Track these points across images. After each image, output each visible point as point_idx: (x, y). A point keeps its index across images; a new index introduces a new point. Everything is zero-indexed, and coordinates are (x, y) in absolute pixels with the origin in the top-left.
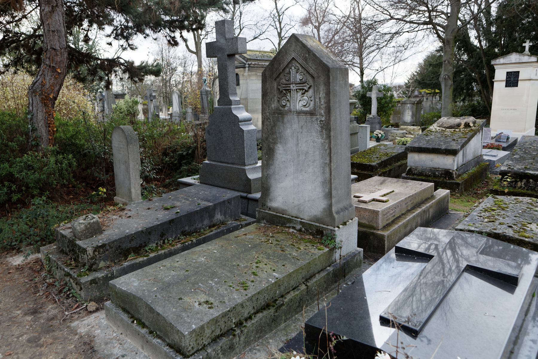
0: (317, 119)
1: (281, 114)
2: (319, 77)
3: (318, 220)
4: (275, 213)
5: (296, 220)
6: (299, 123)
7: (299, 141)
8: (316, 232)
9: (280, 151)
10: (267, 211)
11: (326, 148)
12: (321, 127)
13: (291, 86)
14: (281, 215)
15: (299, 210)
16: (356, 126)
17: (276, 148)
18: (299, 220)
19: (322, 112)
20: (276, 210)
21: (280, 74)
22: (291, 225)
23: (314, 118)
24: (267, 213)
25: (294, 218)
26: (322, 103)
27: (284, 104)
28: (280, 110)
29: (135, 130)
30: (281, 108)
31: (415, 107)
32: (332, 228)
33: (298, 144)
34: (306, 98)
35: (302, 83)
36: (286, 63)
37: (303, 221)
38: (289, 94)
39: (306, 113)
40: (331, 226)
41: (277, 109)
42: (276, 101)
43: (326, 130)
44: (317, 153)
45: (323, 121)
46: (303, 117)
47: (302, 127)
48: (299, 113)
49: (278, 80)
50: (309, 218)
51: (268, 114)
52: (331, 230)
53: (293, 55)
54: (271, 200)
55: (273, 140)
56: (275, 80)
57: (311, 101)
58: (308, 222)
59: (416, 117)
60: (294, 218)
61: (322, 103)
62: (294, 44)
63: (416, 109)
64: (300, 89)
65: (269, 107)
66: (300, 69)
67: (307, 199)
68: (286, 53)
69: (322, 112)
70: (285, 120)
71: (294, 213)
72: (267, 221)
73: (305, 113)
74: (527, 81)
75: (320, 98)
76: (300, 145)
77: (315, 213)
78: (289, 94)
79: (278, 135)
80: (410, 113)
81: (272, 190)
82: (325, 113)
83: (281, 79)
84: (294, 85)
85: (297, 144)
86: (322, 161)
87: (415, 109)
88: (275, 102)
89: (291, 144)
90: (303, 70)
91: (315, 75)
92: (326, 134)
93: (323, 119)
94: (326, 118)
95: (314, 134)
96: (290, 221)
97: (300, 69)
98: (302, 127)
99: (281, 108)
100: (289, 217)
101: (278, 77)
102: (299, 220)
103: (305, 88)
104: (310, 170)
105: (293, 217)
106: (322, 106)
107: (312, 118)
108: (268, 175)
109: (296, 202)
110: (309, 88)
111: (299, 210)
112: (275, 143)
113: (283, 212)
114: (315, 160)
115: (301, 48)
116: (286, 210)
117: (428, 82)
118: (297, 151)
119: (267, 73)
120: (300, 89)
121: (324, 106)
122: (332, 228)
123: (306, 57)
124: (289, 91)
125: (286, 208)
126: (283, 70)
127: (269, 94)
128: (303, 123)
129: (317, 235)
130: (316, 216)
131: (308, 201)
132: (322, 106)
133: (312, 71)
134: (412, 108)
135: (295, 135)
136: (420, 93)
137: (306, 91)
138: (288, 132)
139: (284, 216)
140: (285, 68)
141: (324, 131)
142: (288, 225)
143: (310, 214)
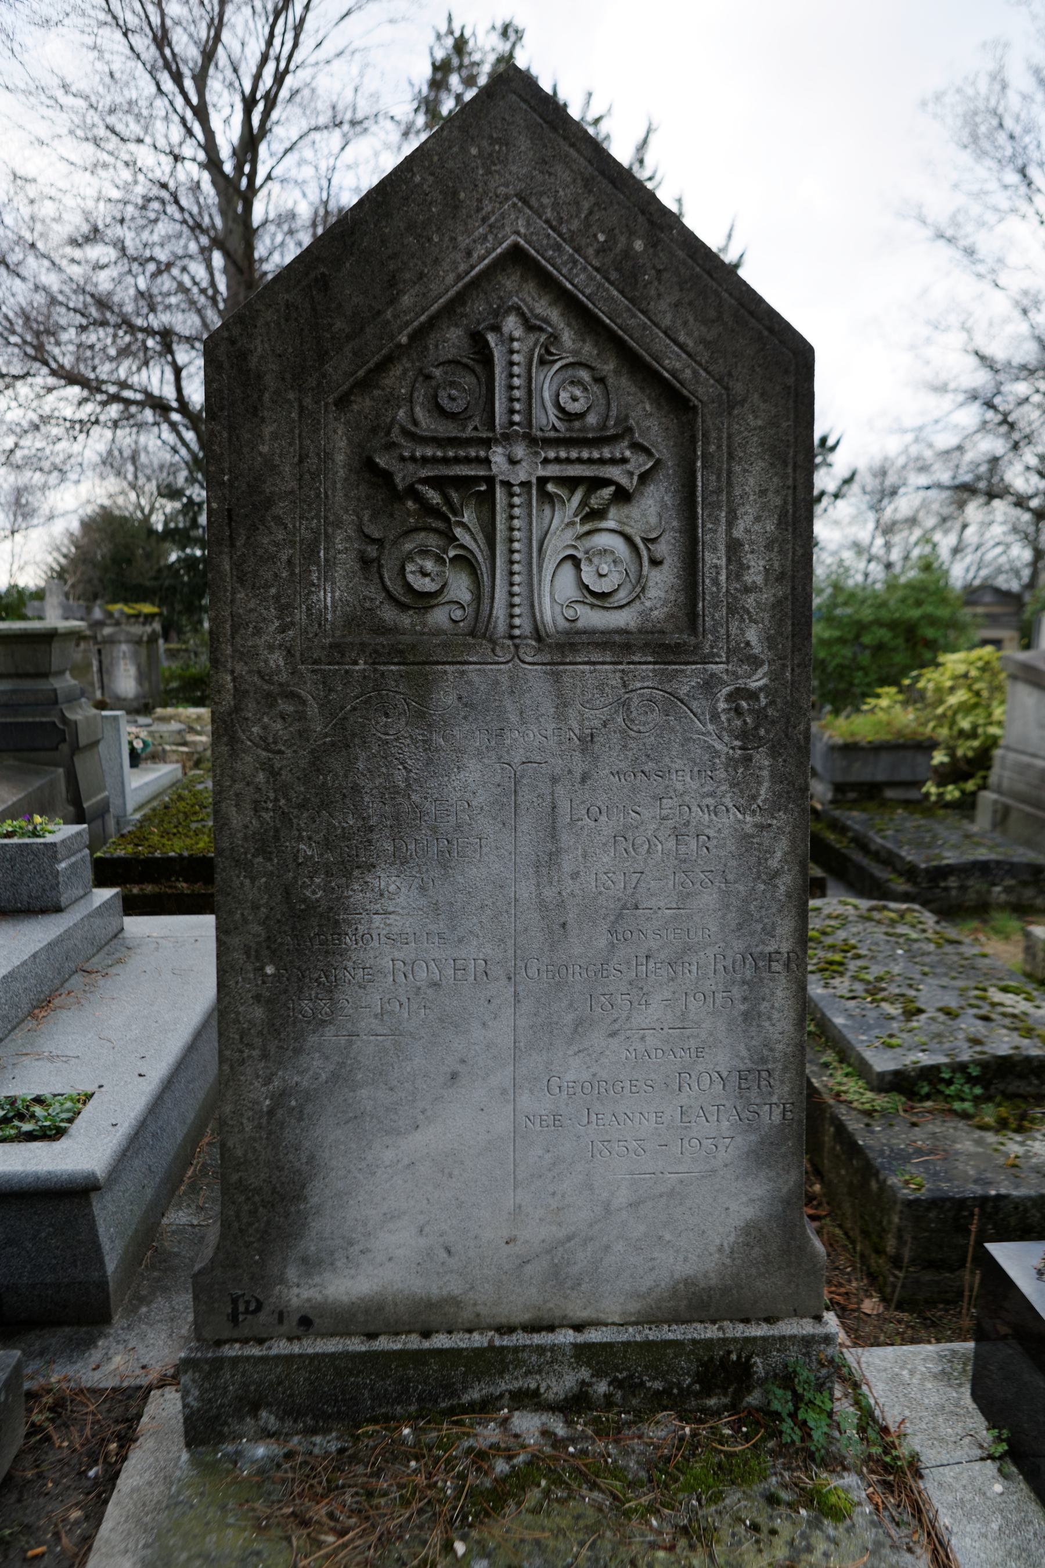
0: (709, 685)
1: (400, 654)
2: (730, 404)
3: (698, 1302)
4: (357, 1345)
5: (541, 1350)
6: (560, 716)
7: (566, 839)
8: (699, 1378)
9: (394, 919)
10: (281, 1347)
11: (774, 863)
12: (744, 735)
13: (498, 456)
14: (414, 1342)
15: (556, 1275)
16: (95, 716)
17: (357, 897)
18: (566, 1337)
19: (752, 635)
20: (368, 1318)
21: (388, 361)
22: (505, 1385)
23: (688, 679)
24: (289, 1359)
25: (520, 1339)
26: (754, 576)
27: (426, 585)
28: (382, 629)
29: (13, 250)
30: (389, 614)
31: (143, 651)
32: (806, 1327)
33: (553, 857)
34: (618, 544)
35: (574, 434)
36: (446, 284)
37: (594, 1336)
38: (468, 516)
39: (627, 647)
40: (797, 1313)
41: (351, 622)
42: (346, 562)
43: (774, 753)
44: (709, 898)
45: (752, 695)
46: (595, 678)
47: (588, 741)
48: (565, 646)
49: (363, 404)
50: (634, 1306)
51: (277, 659)
52: (808, 1341)
53: (518, 230)
54: (311, 1265)
55: (327, 845)
56: (343, 402)
57: (655, 563)
58: (630, 1334)
59: (150, 682)
60: (520, 1339)
61: (754, 576)
62: (523, 143)
63: (149, 657)
64: (571, 483)
65: (285, 609)
66: (567, 337)
67: (622, 1197)
68: (453, 205)
69: (752, 635)
70: (446, 697)
71: (520, 1301)
72: (290, 1412)
73: (618, 645)
74: (557, 577)
75: (734, 547)
76: (567, 864)
77: (683, 1269)
78: (468, 516)
79: (372, 807)
80: (132, 670)
81: (317, 1194)
82: (770, 642)
83: (391, 400)
84: (520, 451)
85: (549, 860)
86: (739, 945)
87: (143, 659)
88: (339, 573)
89: (495, 862)
90: (588, 350)
91: (702, 389)
92: (776, 777)
93: (757, 681)
94: (775, 676)
95: (685, 782)
96: (492, 1362)
97: (567, 337)
98: (588, 741)
99: (389, 614)
100: (478, 1340)
101: (364, 385)
102: (566, 1337)
103: (614, 473)
104: (655, 1012)
105: (511, 1330)
106: (750, 601)
107: (673, 676)
108: (280, 1097)
109: (536, 1233)
110: (644, 478)
111: (556, 1275)
112: (349, 862)
113: (426, 1316)
114: (687, 949)
115: (588, 183)
116: (454, 1301)
117: (148, 583)
118: (542, 905)
119: (259, 347)
120: (571, 483)
121: (766, 596)
122: (806, 1327)
123: (628, 253)
124: (483, 492)
125: (455, 1287)
126: (419, 335)
127: (281, 508)
128: (595, 718)
129: (708, 1391)
130: (688, 1282)
131: (634, 1205)
132: (750, 601)
133: (673, 362)
134: (136, 656)
135: (526, 796)
136: (110, 615)
137: (623, 496)
138: (470, 779)
139: (441, 1341)
140: (432, 323)
141: (762, 759)
142: (474, 1394)
143: (648, 1282)
